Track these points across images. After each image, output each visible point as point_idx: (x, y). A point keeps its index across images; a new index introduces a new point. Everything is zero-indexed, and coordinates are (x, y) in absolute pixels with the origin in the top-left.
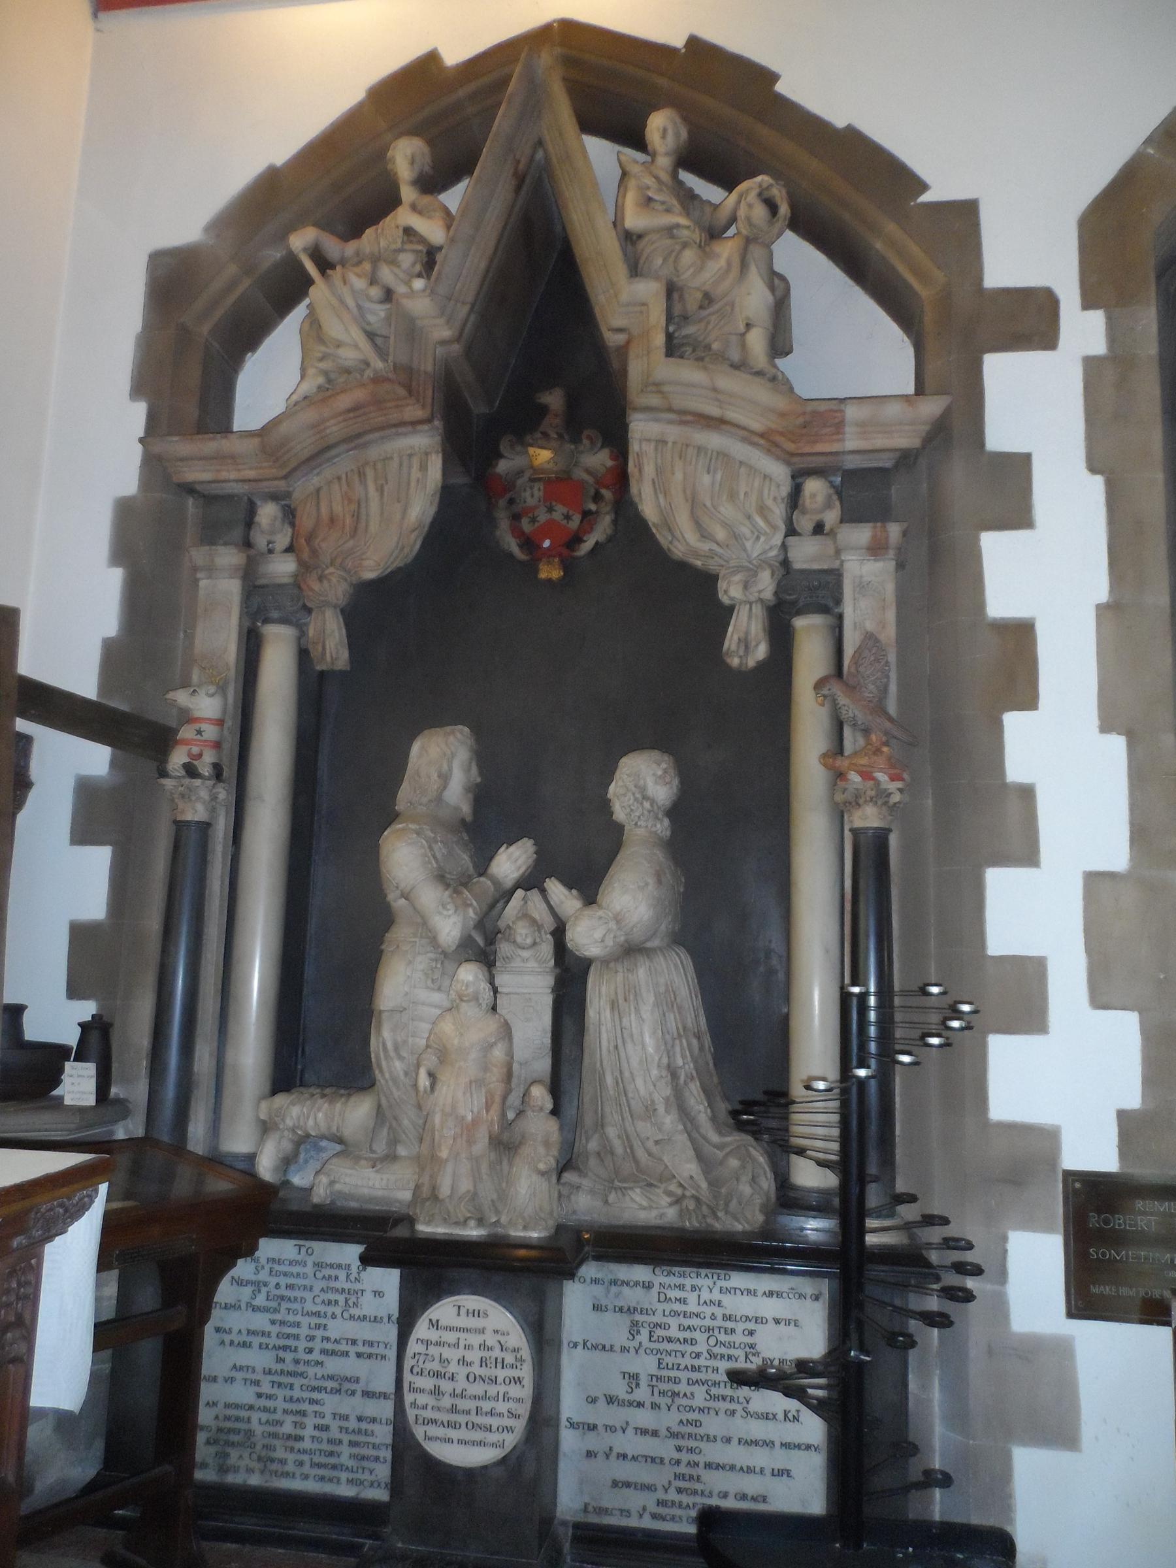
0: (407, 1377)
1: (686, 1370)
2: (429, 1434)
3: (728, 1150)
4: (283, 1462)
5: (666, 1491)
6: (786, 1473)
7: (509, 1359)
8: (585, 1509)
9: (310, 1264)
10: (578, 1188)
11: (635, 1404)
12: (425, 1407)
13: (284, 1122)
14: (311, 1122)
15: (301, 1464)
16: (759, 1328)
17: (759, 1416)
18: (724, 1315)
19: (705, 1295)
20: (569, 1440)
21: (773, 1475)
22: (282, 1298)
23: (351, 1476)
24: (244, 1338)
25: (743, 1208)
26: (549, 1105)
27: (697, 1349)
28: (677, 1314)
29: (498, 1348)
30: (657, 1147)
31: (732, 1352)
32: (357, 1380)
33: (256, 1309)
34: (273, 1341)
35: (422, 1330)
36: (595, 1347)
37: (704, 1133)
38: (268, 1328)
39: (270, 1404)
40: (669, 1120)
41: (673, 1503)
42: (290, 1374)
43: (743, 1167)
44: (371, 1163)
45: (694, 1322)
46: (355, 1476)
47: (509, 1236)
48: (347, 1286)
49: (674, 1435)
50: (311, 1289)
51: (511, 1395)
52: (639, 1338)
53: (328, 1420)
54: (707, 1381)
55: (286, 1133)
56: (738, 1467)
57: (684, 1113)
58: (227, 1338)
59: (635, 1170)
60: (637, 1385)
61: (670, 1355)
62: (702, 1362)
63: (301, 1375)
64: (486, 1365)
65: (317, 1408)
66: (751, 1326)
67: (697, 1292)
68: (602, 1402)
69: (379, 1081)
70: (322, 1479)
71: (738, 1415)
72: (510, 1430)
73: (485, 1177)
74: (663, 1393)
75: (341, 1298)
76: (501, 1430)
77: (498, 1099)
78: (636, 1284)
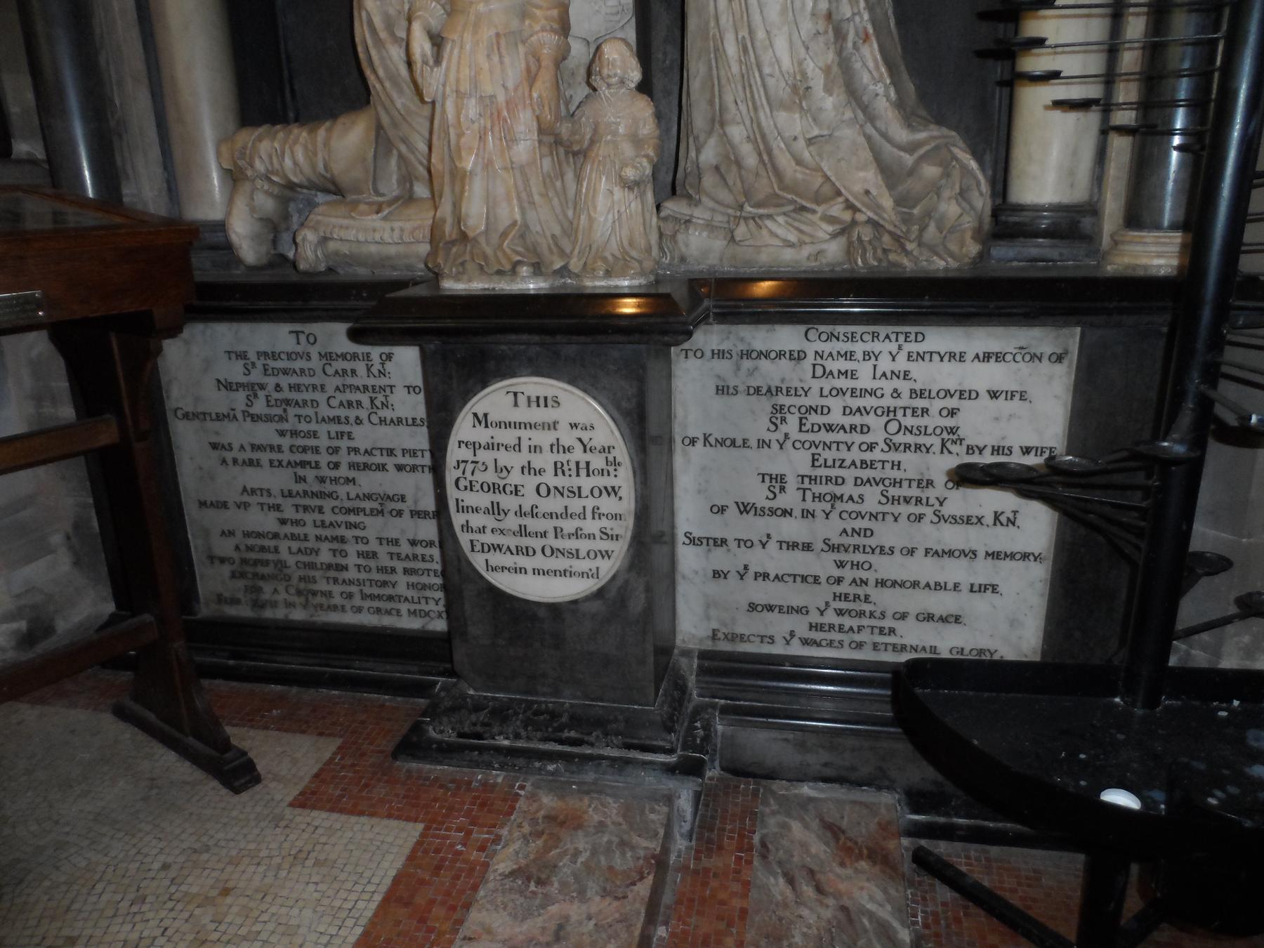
0: (452, 493)
1: (853, 467)
2: (493, 563)
3: (922, 151)
4: (328, 594)
5: (822, 613)
6: (991, 589)
7: (598, 462)
8: (714, 636)
9: (315, 356)
10: (688, 222)
11: (779, 512)
12: (482, 530)
13: (252, 166)
14: (288, 162)
15: (350, 596)
16: (966, 405)
17: (955, 520)
18: (913, 391)
19: (885, 364)
20: (689, 559)
21: (971, 591)
22: (287, 402)
23: (413, 607)
24: (249, 455)
25: (945, 237)
26: (636, 75)
27: (868, 438)
28: (841, 392)
29: (579, 447)
30: (811, 148)
31: (921, 440)
32: (403, 498)
33: (255, 418)
34: (286, 456)
35: (464, 428)
36: (722, 443)
37: (883, 129)
38: (277, 440)
39: (297, 530)
40: (829, 103)
41: (831, 627)
42: (314, 495)
43: (947, 175)
44: (375, 208)
45: (868, 402)
46: (418, 607)
47: (585, 287)
48: (371, 382)
49: (833, 548)
50: (323, 387)
51: (603, 510)
52: (784, 428)
53: (373, 546)
54: (883, 480)
55: (259, 183)
56: (922, 584)
57: (853, 93)
58: (229, 456)
59: (776, 187)
60: (782, 489)
61: (830, 448)
62: (877, 455)
63: (330, 495)
64: (564, 473)
65: (358, 533)
66: (952, 403)
67: (873, 361)
68: (733, 511)
69: (374, 87)
70: (378, 611)
71: (926, 520)
72: (606, 554)
73: (536, 198)
74: (819, 498)
75: (365, 398)
76: (592, 555)
77: (547, 62)
78: (780, 354)
